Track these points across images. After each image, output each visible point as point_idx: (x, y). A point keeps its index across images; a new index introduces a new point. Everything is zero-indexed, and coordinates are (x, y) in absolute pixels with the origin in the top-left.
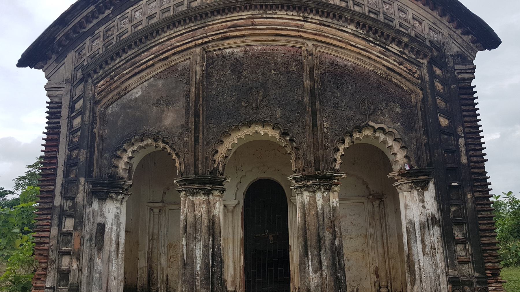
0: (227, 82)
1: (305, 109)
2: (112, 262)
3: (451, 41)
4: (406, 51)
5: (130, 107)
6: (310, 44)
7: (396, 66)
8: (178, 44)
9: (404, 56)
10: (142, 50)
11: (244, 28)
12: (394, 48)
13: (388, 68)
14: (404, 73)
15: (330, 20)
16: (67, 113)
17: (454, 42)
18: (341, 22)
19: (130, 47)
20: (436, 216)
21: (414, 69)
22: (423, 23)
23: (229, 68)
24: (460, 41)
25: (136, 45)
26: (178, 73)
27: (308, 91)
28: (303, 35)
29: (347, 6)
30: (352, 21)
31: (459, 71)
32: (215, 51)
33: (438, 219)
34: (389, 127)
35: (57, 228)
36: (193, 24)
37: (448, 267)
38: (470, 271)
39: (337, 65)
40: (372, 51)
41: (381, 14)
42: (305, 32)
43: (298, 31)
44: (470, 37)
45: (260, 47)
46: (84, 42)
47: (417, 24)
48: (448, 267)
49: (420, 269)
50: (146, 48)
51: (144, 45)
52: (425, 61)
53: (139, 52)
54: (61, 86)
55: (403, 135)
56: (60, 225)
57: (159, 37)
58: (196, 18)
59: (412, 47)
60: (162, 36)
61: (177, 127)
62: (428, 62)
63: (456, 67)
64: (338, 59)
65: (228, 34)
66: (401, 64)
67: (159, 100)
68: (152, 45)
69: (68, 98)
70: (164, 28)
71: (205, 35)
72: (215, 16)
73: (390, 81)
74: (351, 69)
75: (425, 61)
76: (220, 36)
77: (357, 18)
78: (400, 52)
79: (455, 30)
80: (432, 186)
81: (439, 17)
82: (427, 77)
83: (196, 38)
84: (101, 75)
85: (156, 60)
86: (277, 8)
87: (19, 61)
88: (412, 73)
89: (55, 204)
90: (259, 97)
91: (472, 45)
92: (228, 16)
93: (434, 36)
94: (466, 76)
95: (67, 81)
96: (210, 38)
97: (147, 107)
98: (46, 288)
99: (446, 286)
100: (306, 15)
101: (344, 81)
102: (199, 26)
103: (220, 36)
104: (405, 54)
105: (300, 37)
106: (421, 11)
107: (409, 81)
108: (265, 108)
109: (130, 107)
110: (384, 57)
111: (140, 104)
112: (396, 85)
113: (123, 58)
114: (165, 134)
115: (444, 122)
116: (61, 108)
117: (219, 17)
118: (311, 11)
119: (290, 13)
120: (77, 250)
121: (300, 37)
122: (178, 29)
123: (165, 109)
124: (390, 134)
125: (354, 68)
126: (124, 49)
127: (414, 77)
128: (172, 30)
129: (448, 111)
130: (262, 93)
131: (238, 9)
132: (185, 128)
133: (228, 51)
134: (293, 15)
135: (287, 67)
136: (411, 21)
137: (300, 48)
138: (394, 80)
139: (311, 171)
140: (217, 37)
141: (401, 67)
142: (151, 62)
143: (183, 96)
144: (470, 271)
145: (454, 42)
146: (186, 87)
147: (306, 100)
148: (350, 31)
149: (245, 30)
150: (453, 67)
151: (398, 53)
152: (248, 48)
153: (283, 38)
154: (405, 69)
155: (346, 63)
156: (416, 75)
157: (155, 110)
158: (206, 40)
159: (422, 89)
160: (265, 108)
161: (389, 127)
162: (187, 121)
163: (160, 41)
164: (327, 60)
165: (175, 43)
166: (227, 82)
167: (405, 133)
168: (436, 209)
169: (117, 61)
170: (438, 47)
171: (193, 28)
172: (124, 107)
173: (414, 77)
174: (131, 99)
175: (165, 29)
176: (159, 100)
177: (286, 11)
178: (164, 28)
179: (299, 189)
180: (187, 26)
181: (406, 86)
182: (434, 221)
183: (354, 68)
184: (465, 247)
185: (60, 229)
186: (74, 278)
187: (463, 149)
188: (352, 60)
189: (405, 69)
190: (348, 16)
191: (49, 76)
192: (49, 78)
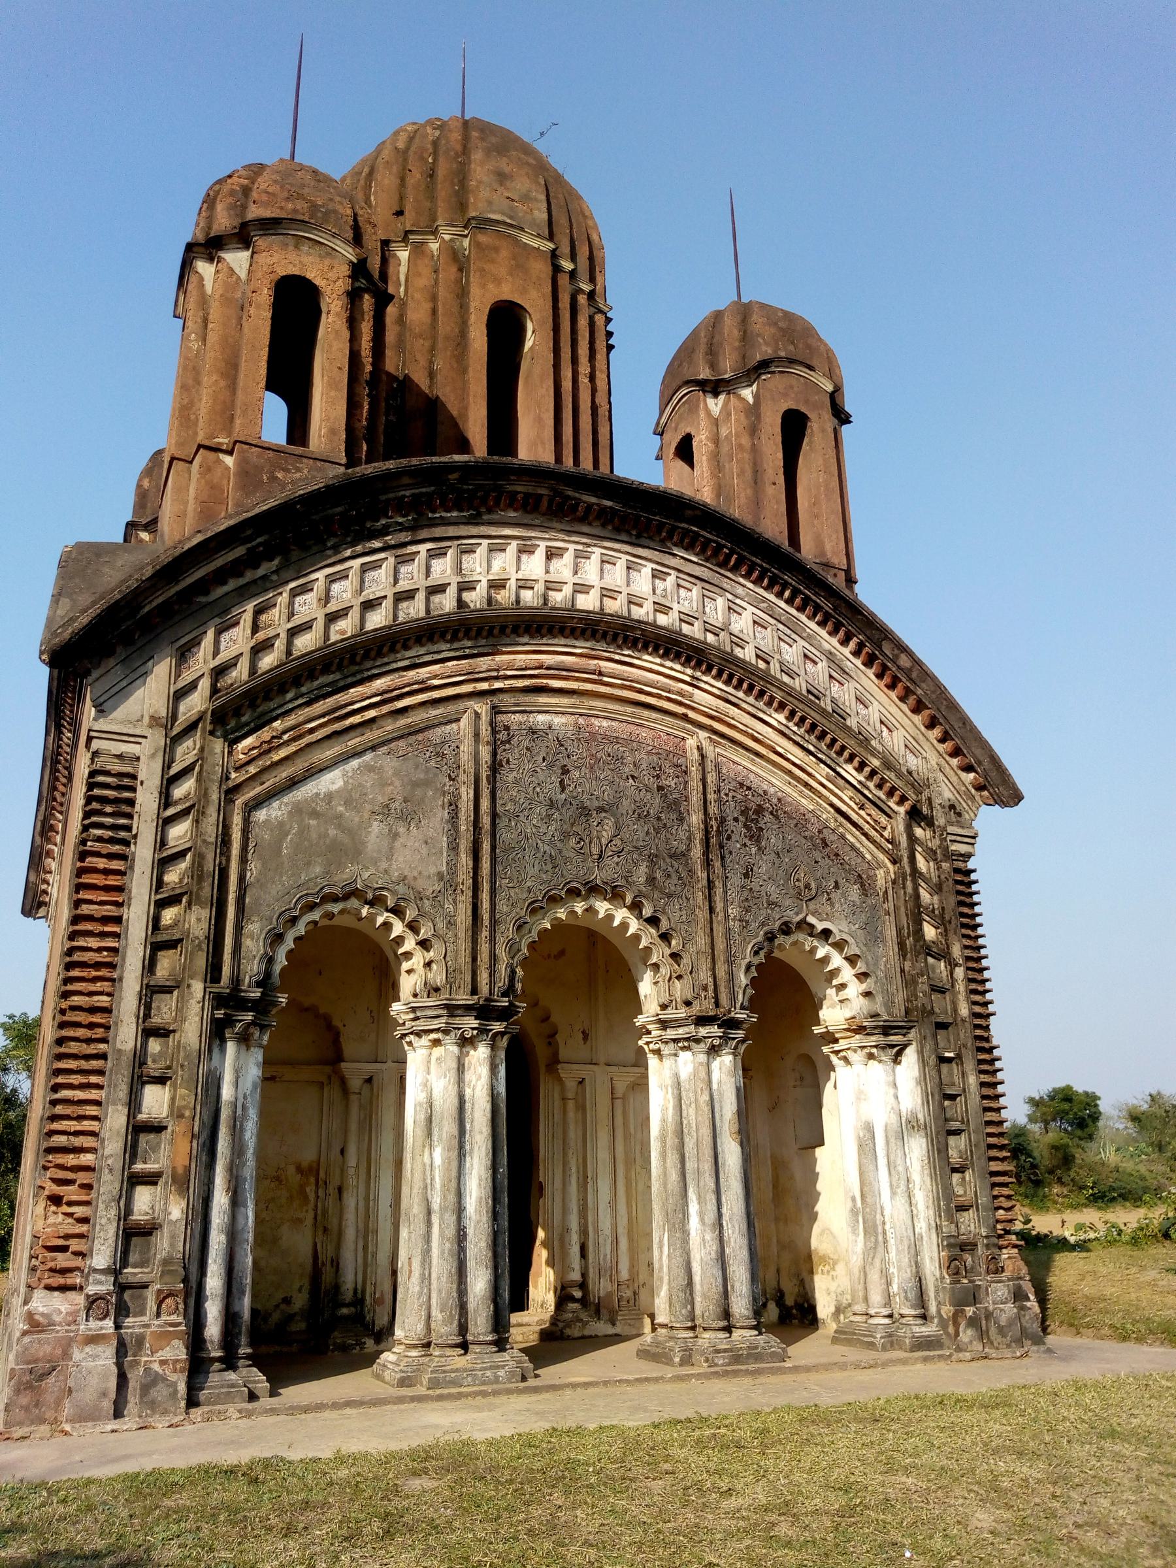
0: (538, 789)
1: (691, 872)
2: (246, 1206)
3: (941, 777)
4: (871, 785)
5: (314, 814)
6: (703, 735)
7: (853, 810)
8: (436, 682)
9: (866, 792)
10: (350, 680)
11: (577, 675)
12: (849, 771)
13: (838, 811)
14: (866, 827)
15: (741, 694)
16: (156, 805)
17: (947, 783)
18: (761, 704)
19: (326, 670)
20: (921, 1116)
21: (883, 819)
22: (895, 733)
23: (544, 759)
24: (954, 779)
25: (340, 668)
26: (431, 749)
27: (699, 836)
28: (691, 714)
29: (769, 669)
30: (781, 707)
31: (954, 838)
32: (514, 712)
33: (922, 1121)
34: (841, 931)
35: (126, 1111)
36: (469, 644)
37: (940, 1216)
38: (972, 1225)
39: (749, 788)
40: (814, 773)
41: (828, 700)
42: (693, 709)
43: (680, 704)
44: (972, 775)
45: (605, 723)
46: (202, 629)
47: (885, 732)
48: (940, 1216)
49: (884, 1223)
50: (359, 677)
51: (357, 668)
52: (901, 810)
53: (342, 684)
54: (138, 732)
55: (864, 949)
56: (134, 1103)
57: (392, 657)
58: (479, 634)
59: (883, 778)
60: (399, 656)
61: (429, 877)
62: (907, 813)
63: (950, 829)
64: (752, 776)
65: (545, 681)
66: (862, 807)
67: (387, 806)
68: (376, 671)
69: (157, 765)
70: (409, 639)
71: (495, 674)
72: (519, 636)
73: (843, 837)
74: (775, 801)
75: (901, 810)
76: (527, 682)
77: (792, 704)
78: (860, 782)
79: (948, 758)
80: (910, 1056)
81: (923, 728)
82: (904, 841)
83: (477, 676)
84: (247, 724)
85: (386, 709)
86: (645, 648)
87: (1004, 804)
88: (880, 829)
89: (119, 1046)
90: (605, 834)
91: (973, 791)
92: (545, 641)
93: (913, 762)
94: (963, 849)
95: (155, 721)
96: (507, 682)
97: (357, 819)
98: (96, 1271)
99: (936, 1255)
100: (698, 674)
101: (762, 825)
102: (481, 650)
103: (527, 682)
104: (868, 788)
105: (685, 718)
106: (894, 710)
107: (874, 842)
108: (616, 859)
109: (314, 814)
110: (337, 714)
111: (341, 809)
112: (853, 847)
113: (304, 689)
114: (402, 889)
115: (930, 932)
116: (133, 789)
117: (525, 639)
118: (708, 671)
119: (669, 664)
120: (180, 1170)
121: (685, 718)
122: (435, 648)
123: (401, 830)
124: (839, 946)
125: (779, 800)
126: (315, 669)
127: (882, 836)
128: (422, 645)
129: (937, 912)
130: (611, 824)
131: (567, 631)
132: (449, 882)
133: (541, 718)
134: (672, 669)
135: (658, 777)
136: (878, 724)
137: (683, 739)
138: (849, 837)
139: (705, 1006)
140: (521, 683)
141: (862, 812)
142: (372, 713)
143: (443, 806)
144: (972, 1225)
145: (947, 783)
146: (449, 786)
147: (697, 852)
148: (775, 723)
149: (577, 679)
150: (944, 829)
151: (855, 783)
152: (581, 721)
153: (655, 715)
154: (868, 818)
155: (765, 787)
156: (886, 834)
157: (376, 828)
158: (498, 685)
159: (894, 862)
160: (616, 859)
161: (841, 931)
162: (452, 866)
163: (394, 666)
164: (732, 775)
165: (429, 679)
166: (538, 789)
167: (865, 945)
168: (920, 1102)
169: (290, 696)
170: (919, 785)
171: (467, 651)
172: (298, 810)
173: (882, 836)
174: (317, 794)
175: (411, 643)
176: (387, 806)
177: (661, 657)
178: (409, 639)
179: (671, 1045)
180: (456, 645)
181: (868, 850)
182: (912, 1125)
183: (779, 800)
184: (964, 1179)
185: (131, 1116)
186: (172, 1245)
187: (961, 987)
188: (778, 783)
189: (868, 818)
190: (779, 696)
191: (102, 700)
192: (101, 705)
